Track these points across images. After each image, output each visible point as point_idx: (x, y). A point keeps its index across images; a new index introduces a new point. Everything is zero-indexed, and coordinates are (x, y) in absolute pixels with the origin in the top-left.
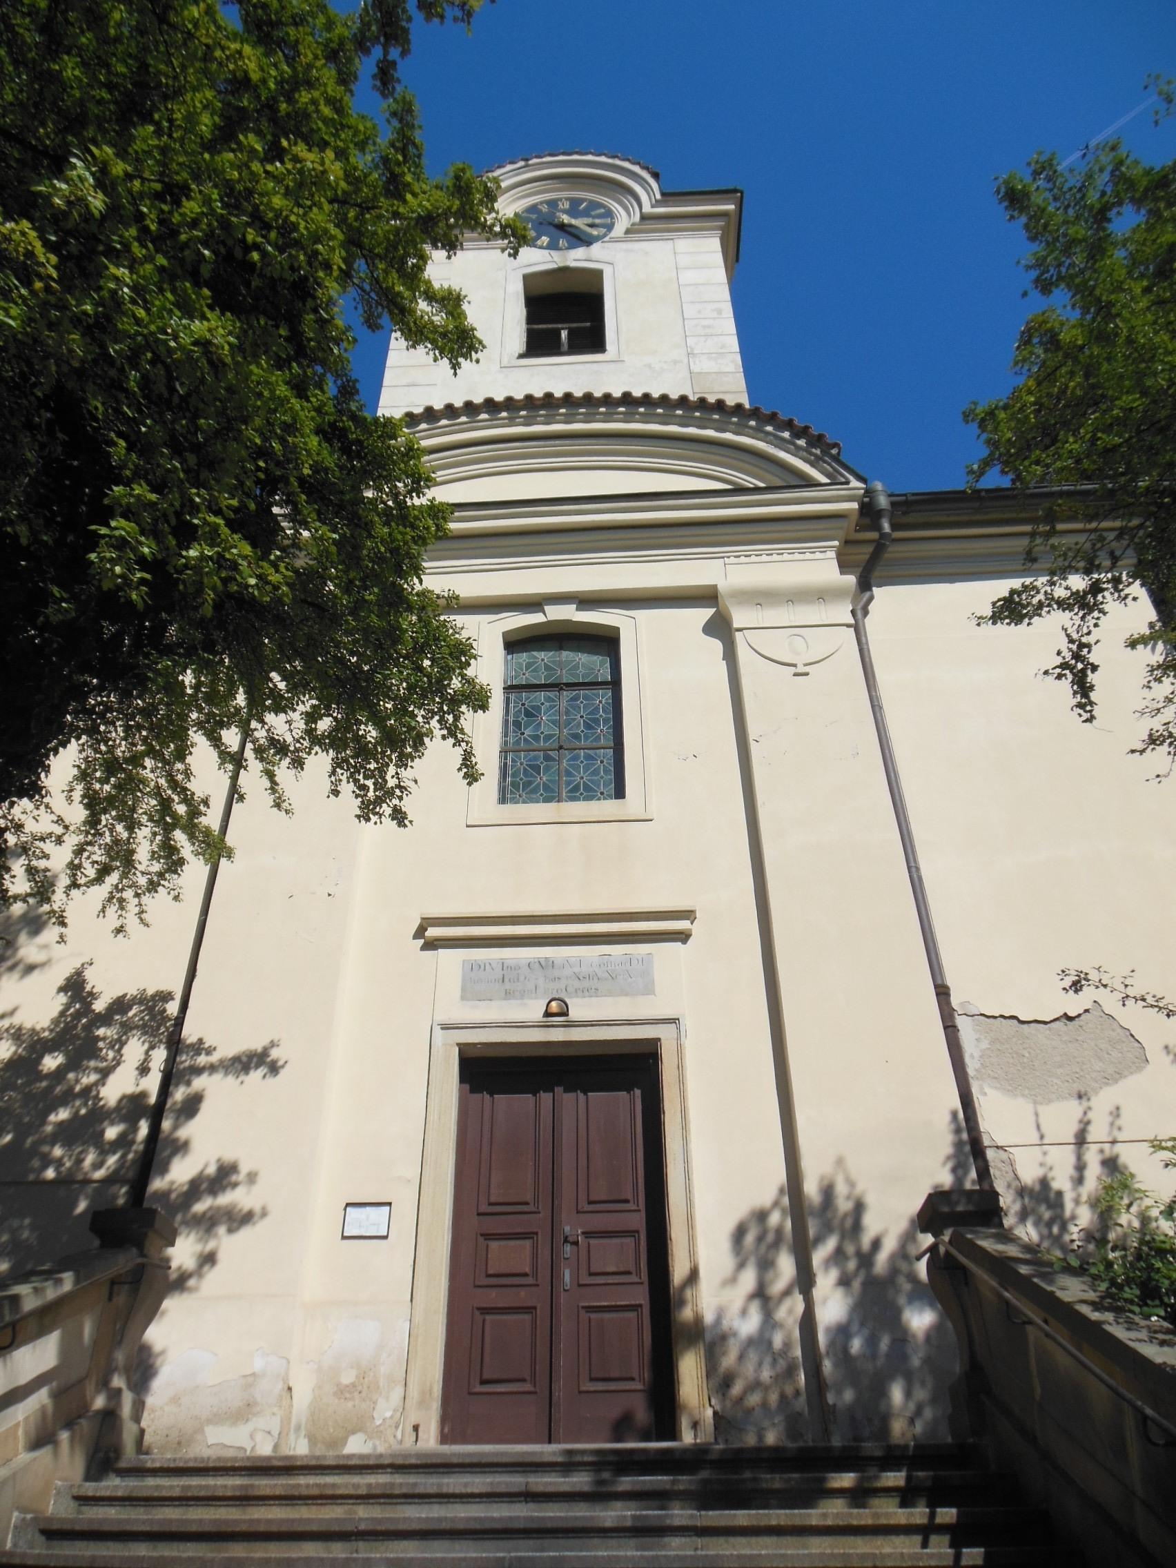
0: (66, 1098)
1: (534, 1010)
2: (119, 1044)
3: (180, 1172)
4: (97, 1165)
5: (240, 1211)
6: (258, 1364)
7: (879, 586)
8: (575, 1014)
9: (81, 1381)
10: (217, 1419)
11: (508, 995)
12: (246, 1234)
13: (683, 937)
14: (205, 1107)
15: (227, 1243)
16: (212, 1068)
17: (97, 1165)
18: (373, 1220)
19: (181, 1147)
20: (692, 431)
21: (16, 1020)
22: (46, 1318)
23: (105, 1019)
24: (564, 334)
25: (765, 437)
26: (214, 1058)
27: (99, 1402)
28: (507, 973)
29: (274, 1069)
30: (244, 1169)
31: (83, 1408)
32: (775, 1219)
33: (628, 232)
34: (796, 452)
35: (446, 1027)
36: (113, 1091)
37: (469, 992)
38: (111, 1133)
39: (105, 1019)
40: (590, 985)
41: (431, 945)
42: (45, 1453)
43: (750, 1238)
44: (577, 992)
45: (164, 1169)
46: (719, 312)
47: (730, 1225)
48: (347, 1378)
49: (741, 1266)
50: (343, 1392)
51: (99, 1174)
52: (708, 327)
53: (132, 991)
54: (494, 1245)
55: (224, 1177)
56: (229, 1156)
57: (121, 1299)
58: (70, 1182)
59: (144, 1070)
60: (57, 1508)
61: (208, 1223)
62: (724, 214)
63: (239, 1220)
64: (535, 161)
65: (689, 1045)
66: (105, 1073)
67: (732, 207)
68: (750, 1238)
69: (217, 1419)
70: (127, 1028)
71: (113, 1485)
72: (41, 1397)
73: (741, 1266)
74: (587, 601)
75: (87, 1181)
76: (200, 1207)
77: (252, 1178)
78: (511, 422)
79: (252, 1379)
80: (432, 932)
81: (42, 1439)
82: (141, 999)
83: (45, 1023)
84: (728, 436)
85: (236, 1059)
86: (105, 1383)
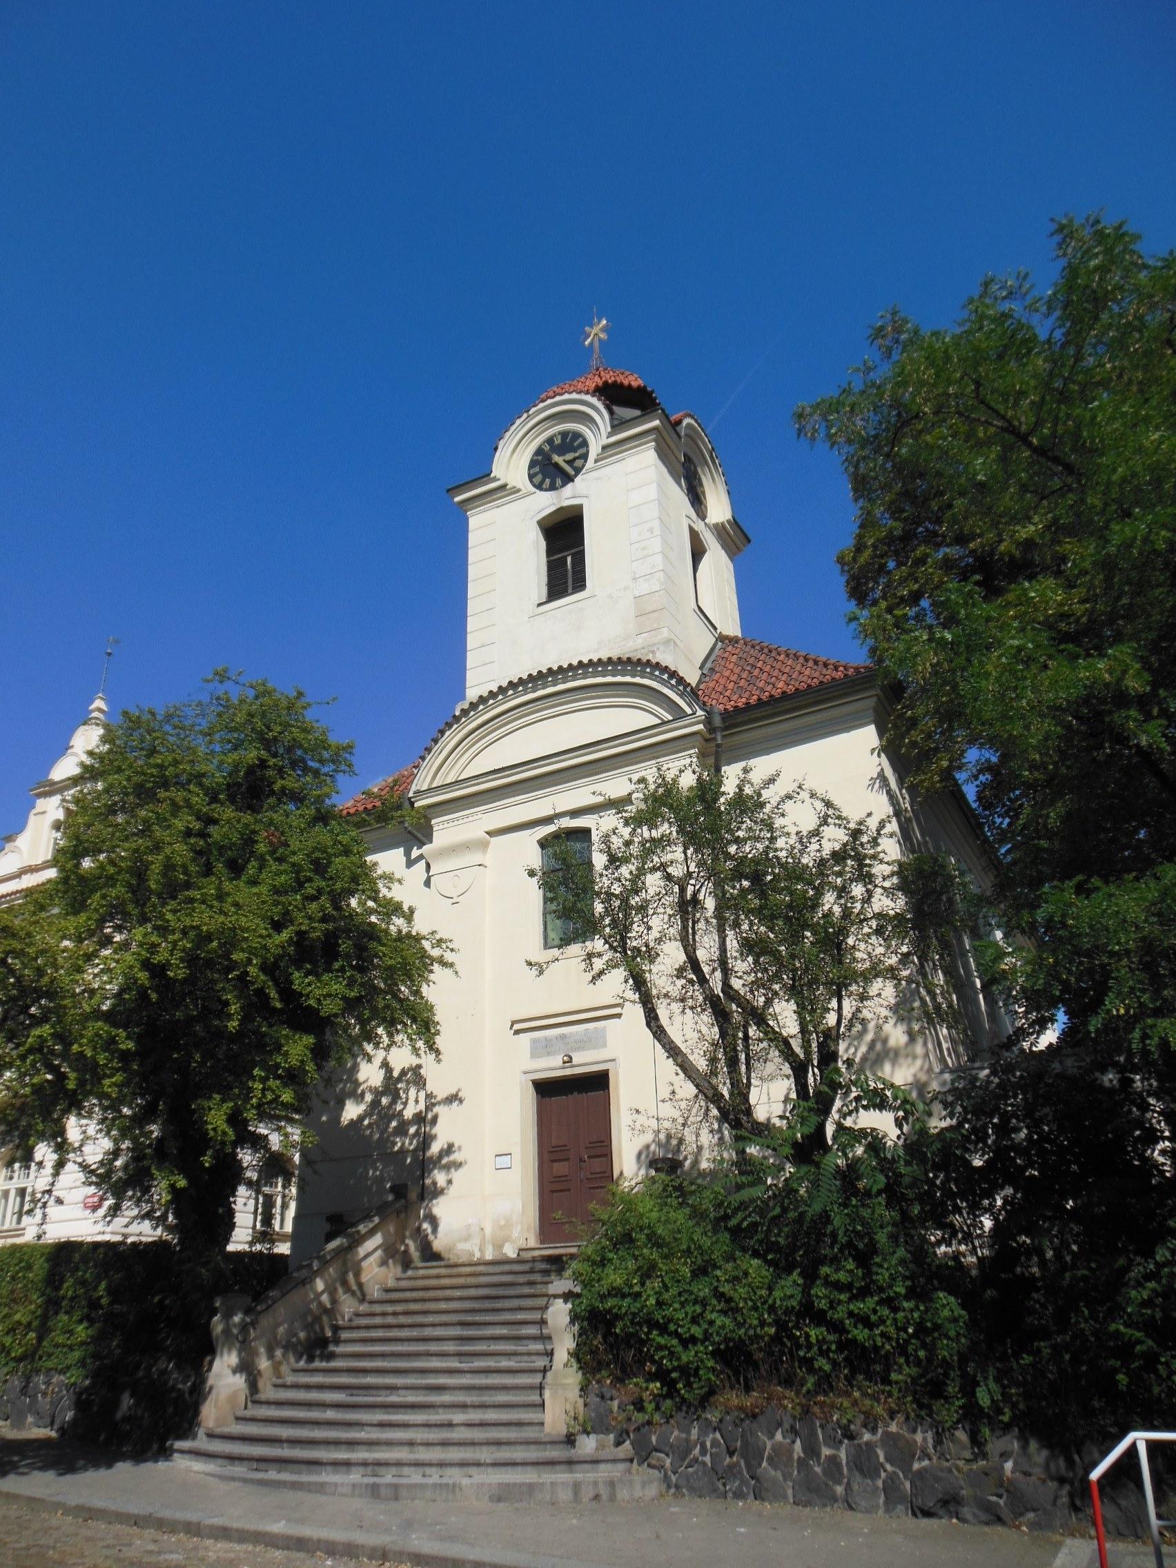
0: (393, 1117)
1: (557, 1061)
2: (407, 1091)
3: (435, 1148)
4: (411, 1144)
5: (222, 1355)
6: (470, 1221)
7: (729, 764)
8: (575, 1061)
9: (394, 1243)
10: (460, 1240)
11: (549, 1054)
12: (461, 1171)
13: (619, 1016)
14: (439, 1120)
15: (456, 1175)
16: (439, 1103)
17: (411, 1144)
18: (505, 1161)
19: (433, 1137)
20: (619, 679)
21: (369, 1084)
22: (372, 1233)
23: (399, 1079)
24: (569, 559)
25: (656, 679)
26: (439, 1099)
27: (403, 1248)
28: (548, 1042)
29: (461, 1101)
30: (456, 1146)
31: (397, 1251)
32: (653, 1147)
33: (596, 461)
34: (672, 688)
35: (525, 1073)
36: (409, 1113)
37: (534, 1055)
38: (412, 1130)
39: (399, 1079)
40: (583, 1044)
41: (517, 1032)
42: (384, 1269)
43: (643, 1156)
44: (578, 1049)
45: (429, 1147)
46: (651, 530)
47: (635, 1152)
48: (502, 1223)
49: (639, 1169)
50: (501, 1228)
51: (412, 1148)
52: (644, 549)
53: (407, 1066)
54: (555, 1165)
55: (449, 1150)
56: (451, 1141)
57: (403, 1216)
58: (403, 1151)
59: (417, 1101)
60: (391, 1283)
61: (447, 1167)
62: (655, 429)
63: (458, 1165)
64: (533, 410)
65: (621, 1071)
66: (405, 1104)
67: (657, 423)
68: (643, 1156)
69: (460, 1240)
70: (408, 1082)
71: (410, 1273)
72: (379, 1253)
73: (639, 1169)
74: (575, 813)
75: (408, 1151)
76: (444, 1161)
77: (460, 1148)
78: (525, 692)
79: (469, 1226)
80: (516, 1027)
81: (383, 1263)
82: (411, 1069)
83: (379, 1084)
84: (638, 680)
85: (447, 1098)
86: (403, 1242)
